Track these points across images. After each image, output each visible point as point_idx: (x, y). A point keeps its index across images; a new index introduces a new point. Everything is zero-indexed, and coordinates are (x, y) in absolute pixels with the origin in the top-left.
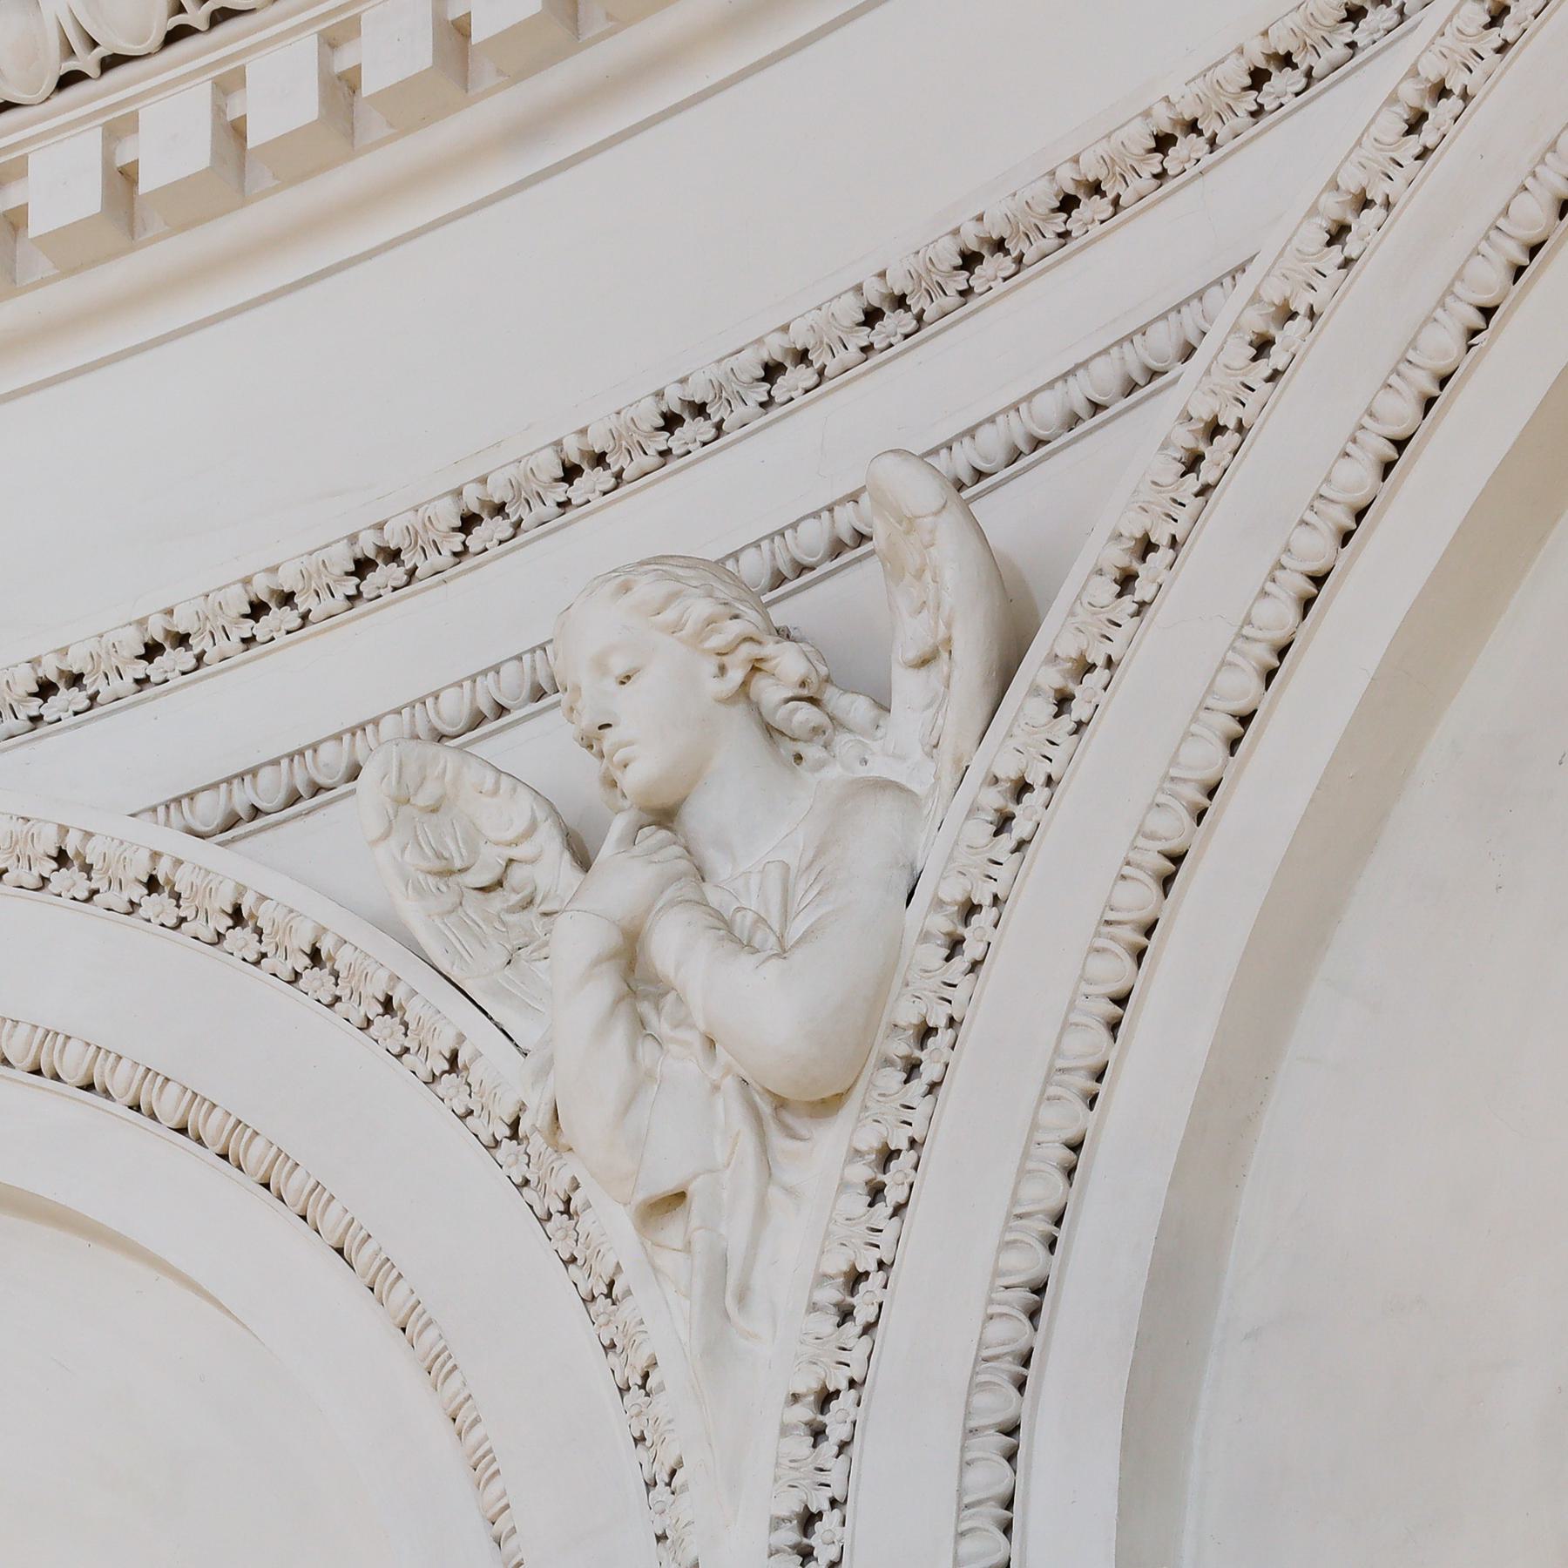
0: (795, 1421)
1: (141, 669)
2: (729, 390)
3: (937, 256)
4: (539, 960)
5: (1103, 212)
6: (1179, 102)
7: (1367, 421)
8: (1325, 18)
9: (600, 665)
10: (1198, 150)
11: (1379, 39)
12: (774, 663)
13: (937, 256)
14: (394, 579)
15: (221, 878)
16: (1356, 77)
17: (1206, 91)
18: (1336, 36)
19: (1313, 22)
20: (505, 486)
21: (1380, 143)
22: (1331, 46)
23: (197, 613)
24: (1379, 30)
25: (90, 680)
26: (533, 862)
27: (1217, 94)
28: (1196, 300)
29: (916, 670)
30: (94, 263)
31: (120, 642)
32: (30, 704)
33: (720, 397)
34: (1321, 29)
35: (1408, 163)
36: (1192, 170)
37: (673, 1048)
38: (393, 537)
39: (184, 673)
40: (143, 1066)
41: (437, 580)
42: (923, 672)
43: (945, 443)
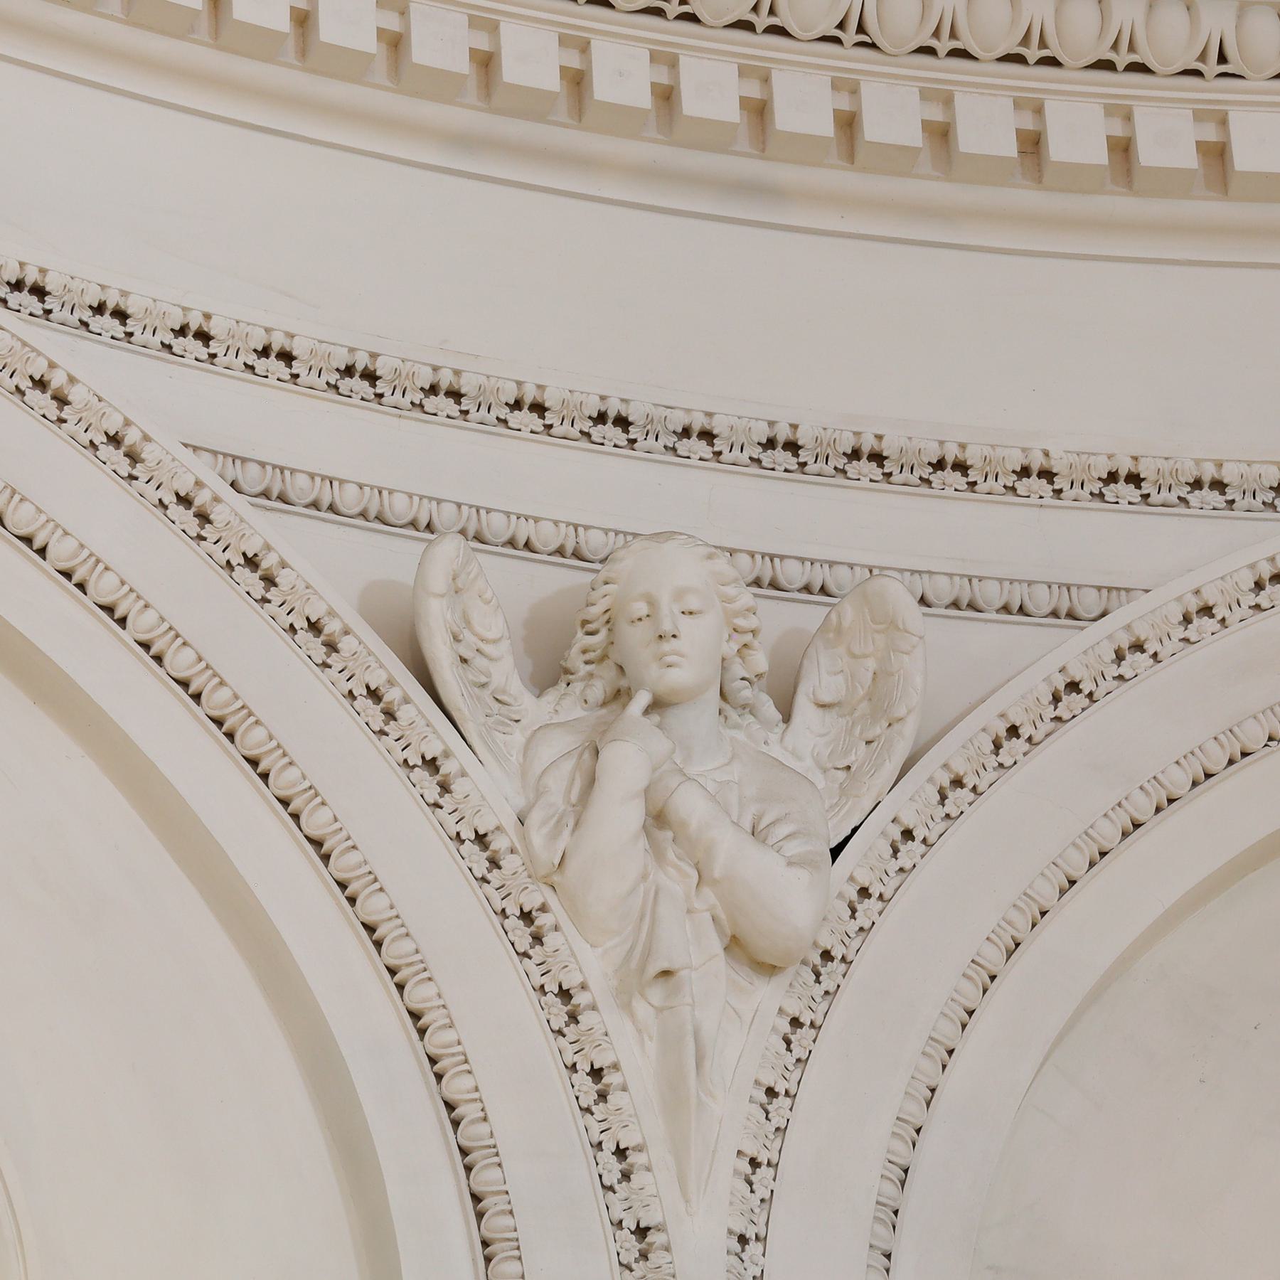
0: (742, 1171)
1: (169, 338)
2: (654, 427)
3: (840, 440)
4: (499, 732)
5: (960, 484)
6: (1056, 459)
7: (1197, 751)
8: (1182, 476)
9: (679, 594)
10: (1045, 492)
11: (1206, 509)
12: (751, 652)
13: (840, 440)
14: (365, 392)
15: (253, 532)
16: (1179, 520)
17: (1078, 464)
18: (1177, 489)
19: (1174, 474)
20: (476, 386)
21: (1237, 586)
22: (1169, 491)
23: (230, 329)
24: (1209, 504)
25: (51, 300)
26: (491, 659)
27: (1083, 470)
28: (1026, 585)
29: (816, 707)
30: (150, 29)
31: (169, 313)
32: (85, 312)
33: (645, 427)
34: (1174, 480)
35: (1245, 608)
36: (1034, 499)
37: (671, 871)
38: (383, 368)
39: (196, 359)
40: (168, 623)
41: (397, 413)
42: (820, 711)
43: (812, 559)
